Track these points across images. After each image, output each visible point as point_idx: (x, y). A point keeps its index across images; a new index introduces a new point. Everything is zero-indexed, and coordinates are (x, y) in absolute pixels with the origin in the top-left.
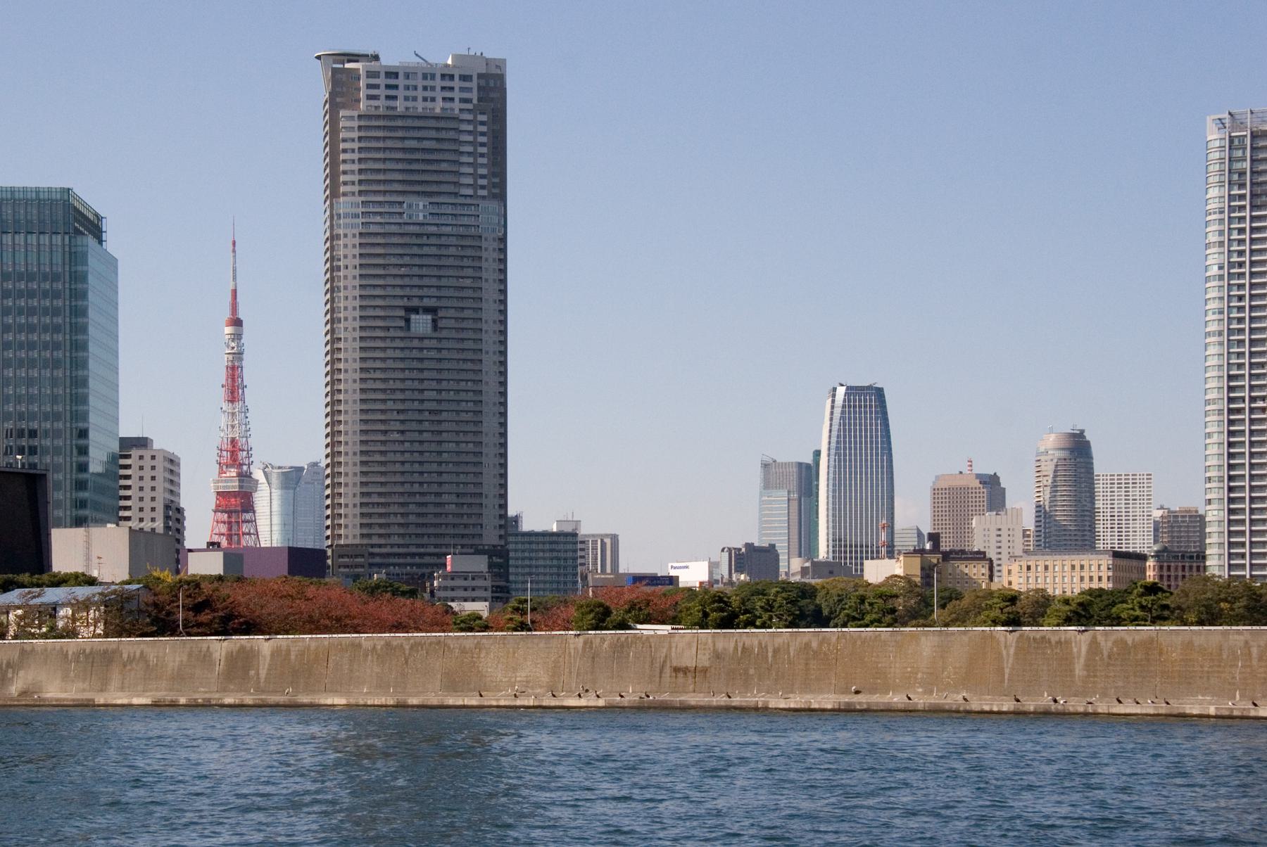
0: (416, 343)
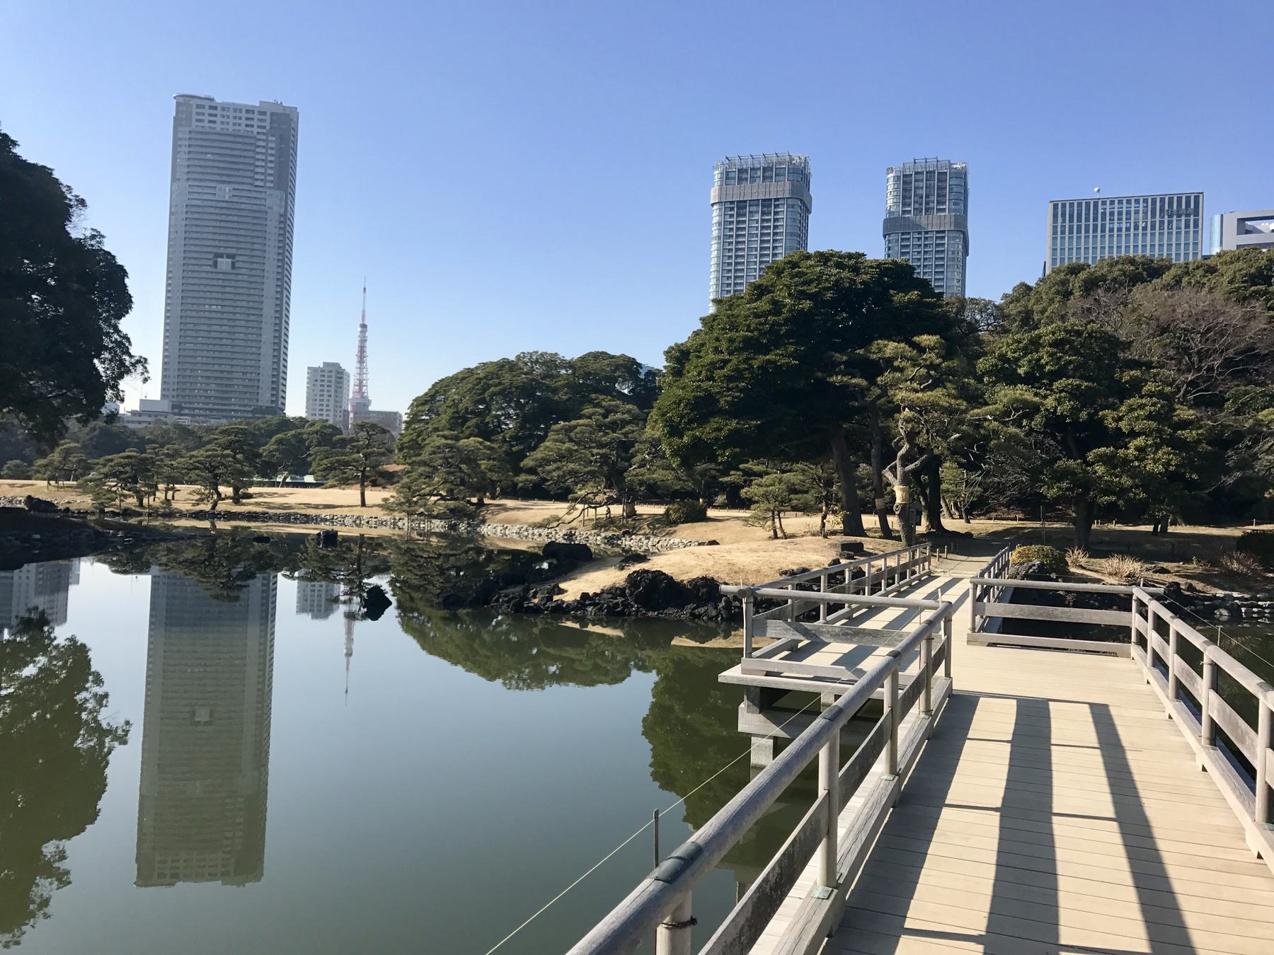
0: (220, 276)
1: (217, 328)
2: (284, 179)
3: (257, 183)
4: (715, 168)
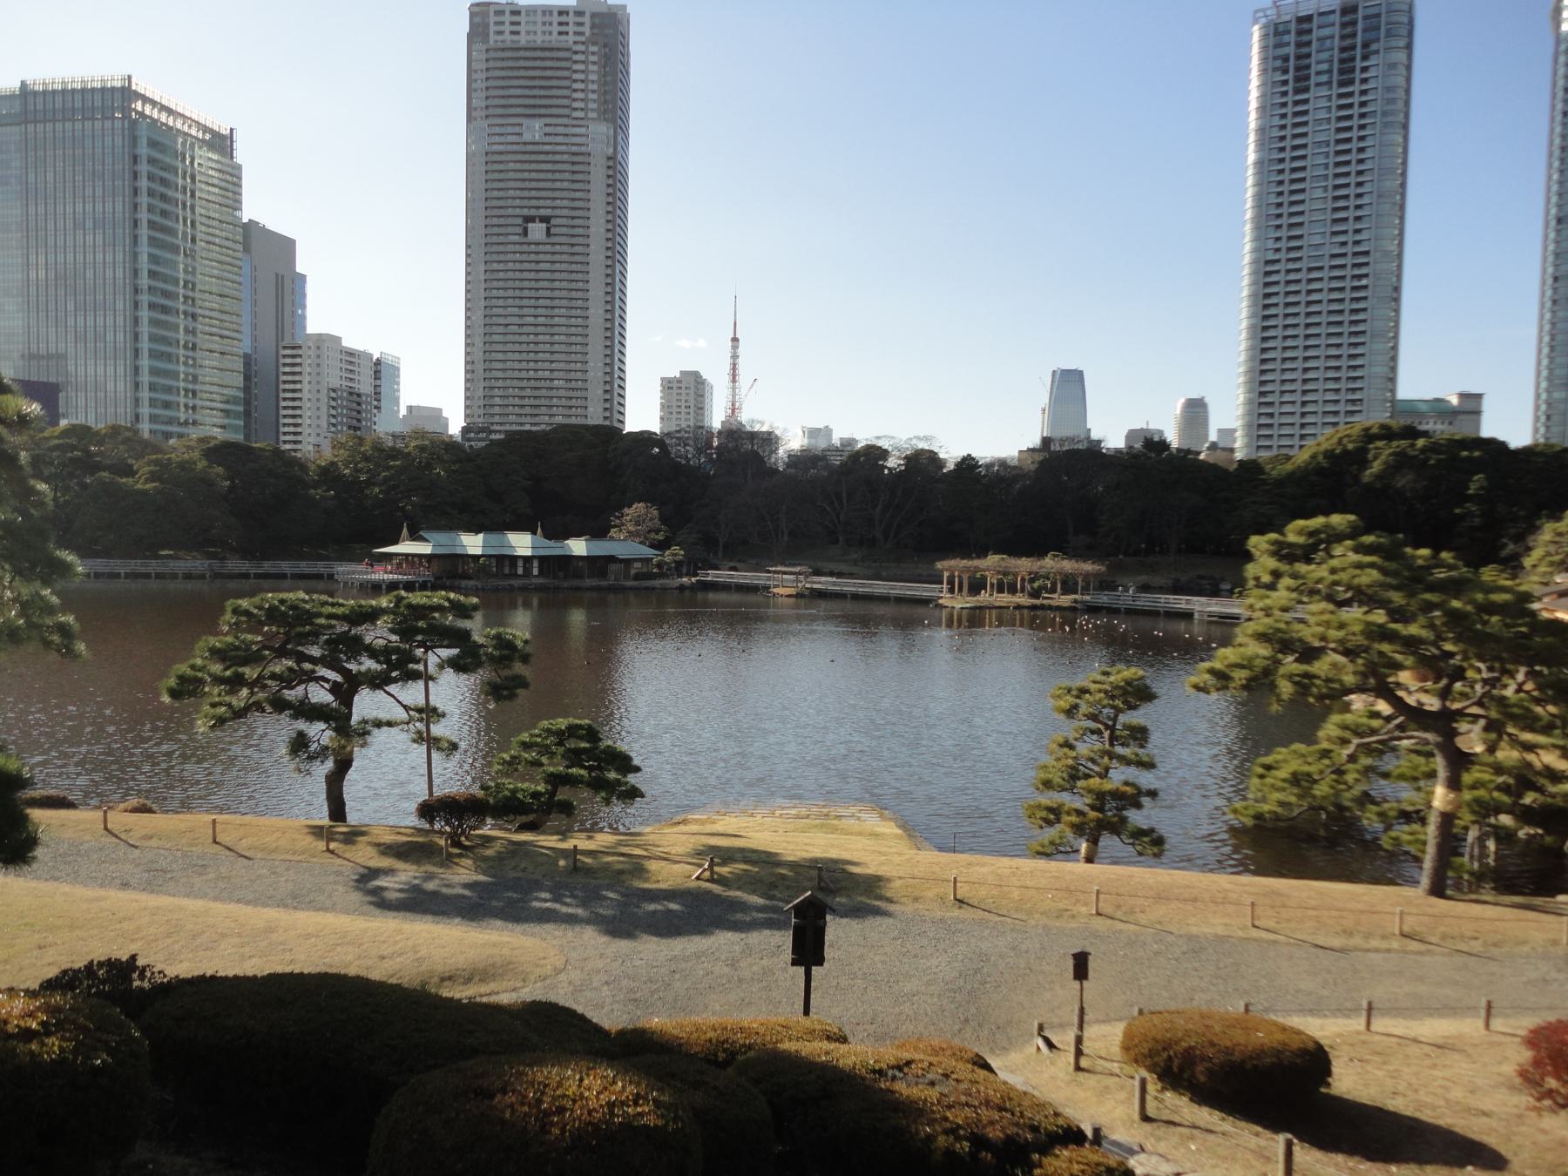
0: (533, 248)
1: (531, 320)
2: (614, 107)
3: (575, 114)
4: (1256, 21)
